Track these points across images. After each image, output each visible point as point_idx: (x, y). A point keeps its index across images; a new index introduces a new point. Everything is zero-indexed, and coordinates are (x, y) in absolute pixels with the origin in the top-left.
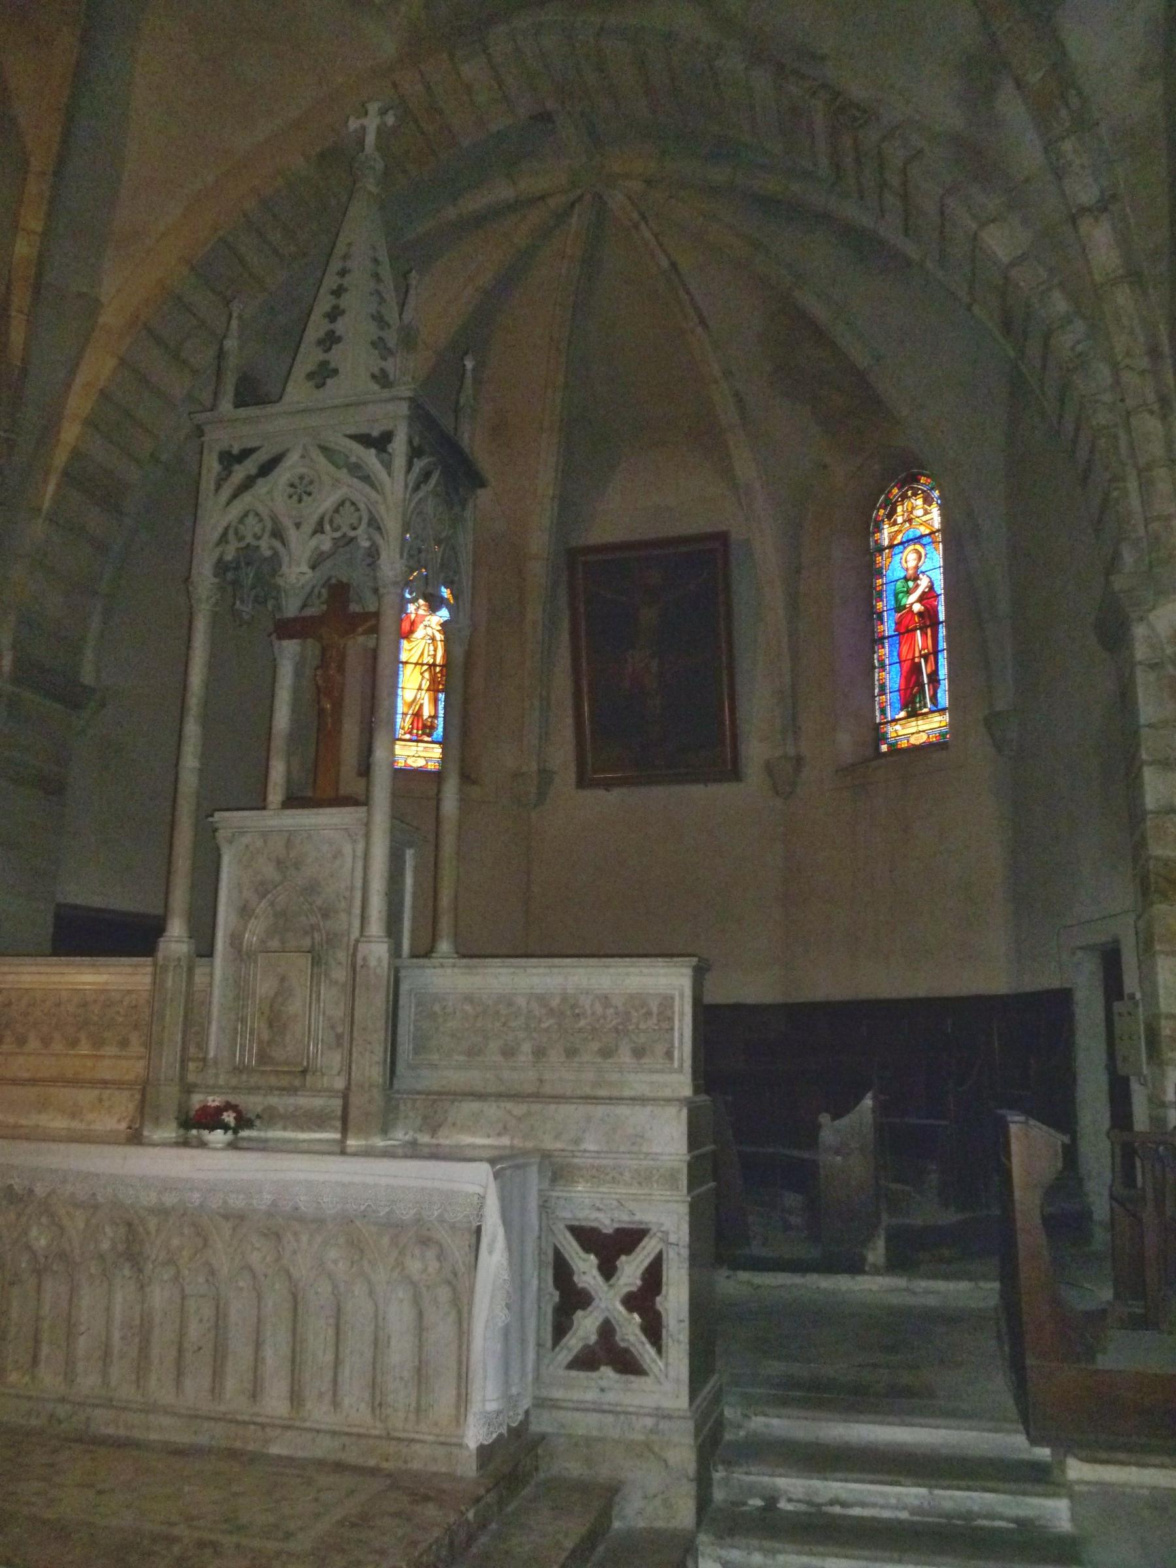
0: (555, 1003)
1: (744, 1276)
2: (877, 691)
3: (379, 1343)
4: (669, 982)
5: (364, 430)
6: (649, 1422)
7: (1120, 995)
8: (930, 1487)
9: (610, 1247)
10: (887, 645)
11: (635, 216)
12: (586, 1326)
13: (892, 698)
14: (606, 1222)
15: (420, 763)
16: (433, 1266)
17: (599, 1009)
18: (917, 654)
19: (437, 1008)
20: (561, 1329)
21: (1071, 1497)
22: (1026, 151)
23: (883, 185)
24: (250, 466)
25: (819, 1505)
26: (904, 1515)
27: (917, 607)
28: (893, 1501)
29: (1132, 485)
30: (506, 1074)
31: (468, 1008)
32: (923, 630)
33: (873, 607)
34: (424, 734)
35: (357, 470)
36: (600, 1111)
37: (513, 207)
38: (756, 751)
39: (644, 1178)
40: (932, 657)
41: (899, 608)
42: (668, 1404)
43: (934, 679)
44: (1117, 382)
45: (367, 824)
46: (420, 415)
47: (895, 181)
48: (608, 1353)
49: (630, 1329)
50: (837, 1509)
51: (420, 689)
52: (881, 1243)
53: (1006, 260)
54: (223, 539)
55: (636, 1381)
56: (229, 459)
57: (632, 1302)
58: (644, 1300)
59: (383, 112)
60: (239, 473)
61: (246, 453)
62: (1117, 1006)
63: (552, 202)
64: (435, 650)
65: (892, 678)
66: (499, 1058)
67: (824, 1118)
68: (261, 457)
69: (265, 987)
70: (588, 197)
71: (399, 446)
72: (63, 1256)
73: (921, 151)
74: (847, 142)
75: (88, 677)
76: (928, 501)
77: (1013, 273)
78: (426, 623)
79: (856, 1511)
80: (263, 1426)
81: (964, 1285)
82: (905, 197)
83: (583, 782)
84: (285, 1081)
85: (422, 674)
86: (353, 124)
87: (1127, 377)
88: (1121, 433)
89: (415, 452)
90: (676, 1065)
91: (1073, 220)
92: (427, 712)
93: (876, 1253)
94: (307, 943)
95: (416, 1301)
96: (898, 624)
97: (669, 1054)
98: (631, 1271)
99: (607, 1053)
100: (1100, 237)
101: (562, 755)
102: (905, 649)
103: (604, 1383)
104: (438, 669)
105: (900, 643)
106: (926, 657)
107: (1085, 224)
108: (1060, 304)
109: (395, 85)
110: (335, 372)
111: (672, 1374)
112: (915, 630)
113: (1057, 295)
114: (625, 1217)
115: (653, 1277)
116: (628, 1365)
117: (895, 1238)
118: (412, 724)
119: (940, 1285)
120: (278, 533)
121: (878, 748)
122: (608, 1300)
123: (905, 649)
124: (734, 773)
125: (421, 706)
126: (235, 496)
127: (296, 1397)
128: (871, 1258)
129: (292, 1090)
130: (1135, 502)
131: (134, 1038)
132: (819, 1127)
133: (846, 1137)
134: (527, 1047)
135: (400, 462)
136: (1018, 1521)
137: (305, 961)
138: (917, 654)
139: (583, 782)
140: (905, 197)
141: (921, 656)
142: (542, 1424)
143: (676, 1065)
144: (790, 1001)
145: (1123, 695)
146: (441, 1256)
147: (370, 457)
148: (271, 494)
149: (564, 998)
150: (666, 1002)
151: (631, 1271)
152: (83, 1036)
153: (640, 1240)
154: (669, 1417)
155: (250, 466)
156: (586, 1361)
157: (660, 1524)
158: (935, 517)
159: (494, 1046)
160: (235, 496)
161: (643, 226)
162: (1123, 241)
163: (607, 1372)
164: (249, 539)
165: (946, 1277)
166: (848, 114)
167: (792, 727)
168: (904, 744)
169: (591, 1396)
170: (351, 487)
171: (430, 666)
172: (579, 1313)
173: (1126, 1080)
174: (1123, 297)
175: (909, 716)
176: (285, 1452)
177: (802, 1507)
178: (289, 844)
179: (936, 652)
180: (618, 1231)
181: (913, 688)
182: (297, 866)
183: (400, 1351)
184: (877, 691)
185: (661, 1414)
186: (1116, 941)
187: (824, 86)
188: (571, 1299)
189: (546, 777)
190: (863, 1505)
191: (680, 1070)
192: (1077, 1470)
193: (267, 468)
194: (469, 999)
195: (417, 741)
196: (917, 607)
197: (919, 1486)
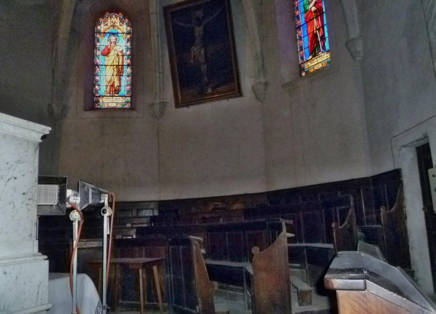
2: (299, 50)
10: (302, 29)
15: (114, 105)
18: (315, 29)
32: (317, 18)
33: (295, 14)
34: (115, 93)
38: (247, 83)
40: (321, 29)
41: (306, 11)
43: (323, 38)
51: (113, 75)
64: (119, 60)
65: (306, 42)
78: (114, 49)
83: (178, 105)
85: (113, 69)
92: (117, 84)
96: (306, 18)
101: (169, 94)
102: (309, 28)
104: (120, 67)
105: (307, 27)
106: (319, 29)
112: (313, 19)
118: (110, 89)
121: (301, 75)
123: (309, 28)
124: (239, 93)
125: (114, 82)
138: (315, 29)
139: (178, 105)
141: (317, 29)
144: (269, 190)
167: (263, 69)
168: (312, 70)
171: (117, 66)
175: (314, 56)
179: (323, 27)
181: (314, 44)
184: (299, 50)
189: (163, 105)
195: (112, 96)
196: (314, 9)
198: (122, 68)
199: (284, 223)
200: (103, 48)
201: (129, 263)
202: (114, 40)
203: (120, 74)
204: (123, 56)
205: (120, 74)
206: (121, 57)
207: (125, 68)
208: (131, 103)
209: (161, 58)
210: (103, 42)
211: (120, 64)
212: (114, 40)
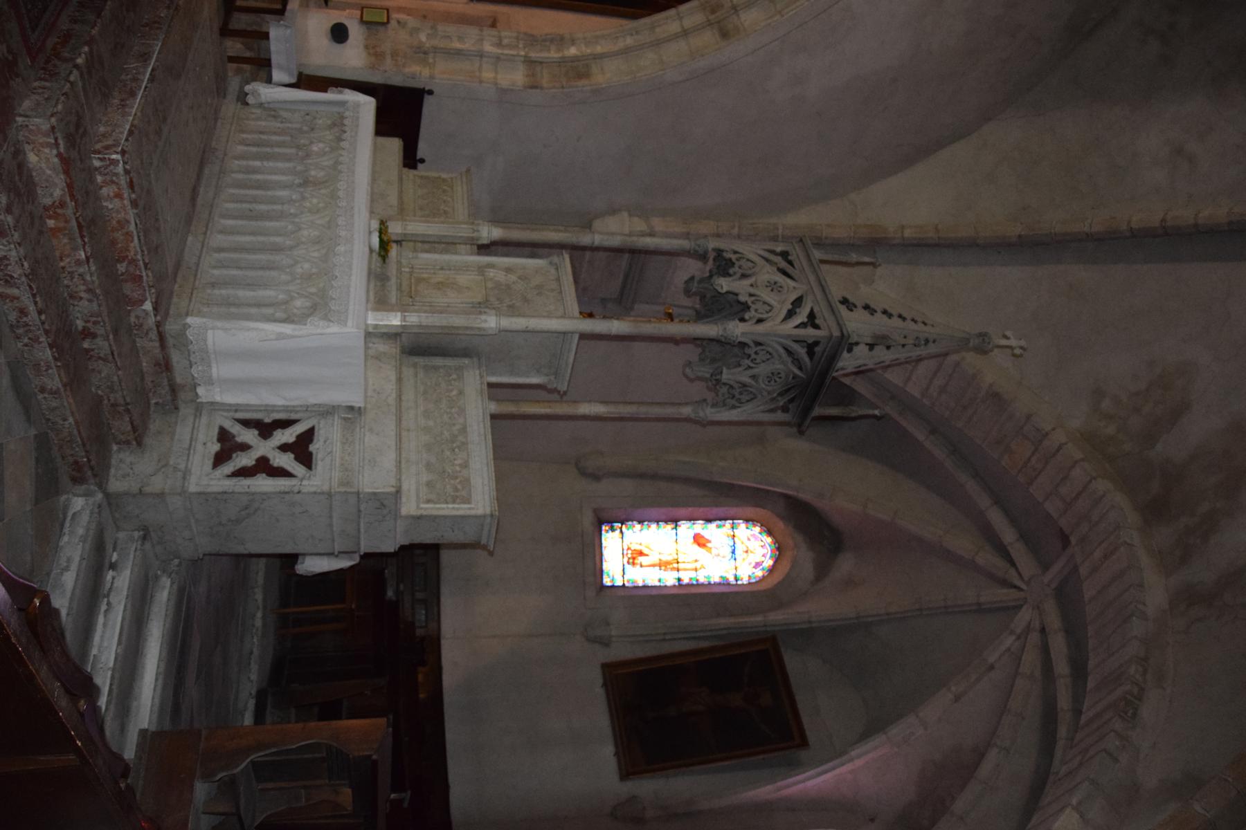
0: (461, 438)
1: (251, 704)
3: (250, 285)
4: (481, 500)
5: (818, 315)
6: (182, 466)
8: (114, 670)
9: (302, 449)
11: (1018, 631)
12: (249, 436)
19: (454, 376)
20: (246, 423)
24: (783, 264)
25: (108, 596)
26: (94, 651)
28: (105, 644)
31: (454, 393)
37: (1002, 550)
48: (228, 447)
49: (245, 460)
50: (104, 607)
55: (209, 462)
56: (785, 255)
58: (264, 467)
60: (778, 259)
61: (790, 263)
63: (1012, 571)
68: (789, 269)
69: (463, 279)
71: (810, 331)
72: (308, 156)
73: (1116, 760)
79: (101, 619)
80: (205, 233)
83: (607, 667)
89: (811, 348)
90: (423, 506)
97: (428, 501)
98: (285, 461)
99: (428, 466)
103: (209, 444)
109: (1054, 429)
111: (212, 483)
114: (320, 456)
120: (744, 276)
122: (265, 448)
129: (399, 288)
134: (431, 423)
135: (802, 332)
139: (607, 667)
143: (423, 506)
147: (802, 317)
148: (768, 274)
153: (302, 462)
154: (184, 478)
156: (224, 436)
157: (113, 471)
161: (1014, 637)
163: (216, 447)
164: (737, 264)
169: (201, 437)
172: (256, 432)
176: (188, 243)
177: (108, 586)
180: (311, 454)
185: (186, 474)
187: (1142, 689)
188: (266, 429)
190: (105, 625)
191: (418, 507)
197: (116, 659)
198: (673, 569)
199: (407, 795)
200: (703, 533)
201: (695, 321)
202: (728, 553)
203: (663, 565)
204: (696, 570)
205: (663, 565)
206: (693, 566)
207: (675, 574)
208: (613, 586)
209: (1064, 702)
210: (716, 533)
211: (681, 566)
212: (728, 553)
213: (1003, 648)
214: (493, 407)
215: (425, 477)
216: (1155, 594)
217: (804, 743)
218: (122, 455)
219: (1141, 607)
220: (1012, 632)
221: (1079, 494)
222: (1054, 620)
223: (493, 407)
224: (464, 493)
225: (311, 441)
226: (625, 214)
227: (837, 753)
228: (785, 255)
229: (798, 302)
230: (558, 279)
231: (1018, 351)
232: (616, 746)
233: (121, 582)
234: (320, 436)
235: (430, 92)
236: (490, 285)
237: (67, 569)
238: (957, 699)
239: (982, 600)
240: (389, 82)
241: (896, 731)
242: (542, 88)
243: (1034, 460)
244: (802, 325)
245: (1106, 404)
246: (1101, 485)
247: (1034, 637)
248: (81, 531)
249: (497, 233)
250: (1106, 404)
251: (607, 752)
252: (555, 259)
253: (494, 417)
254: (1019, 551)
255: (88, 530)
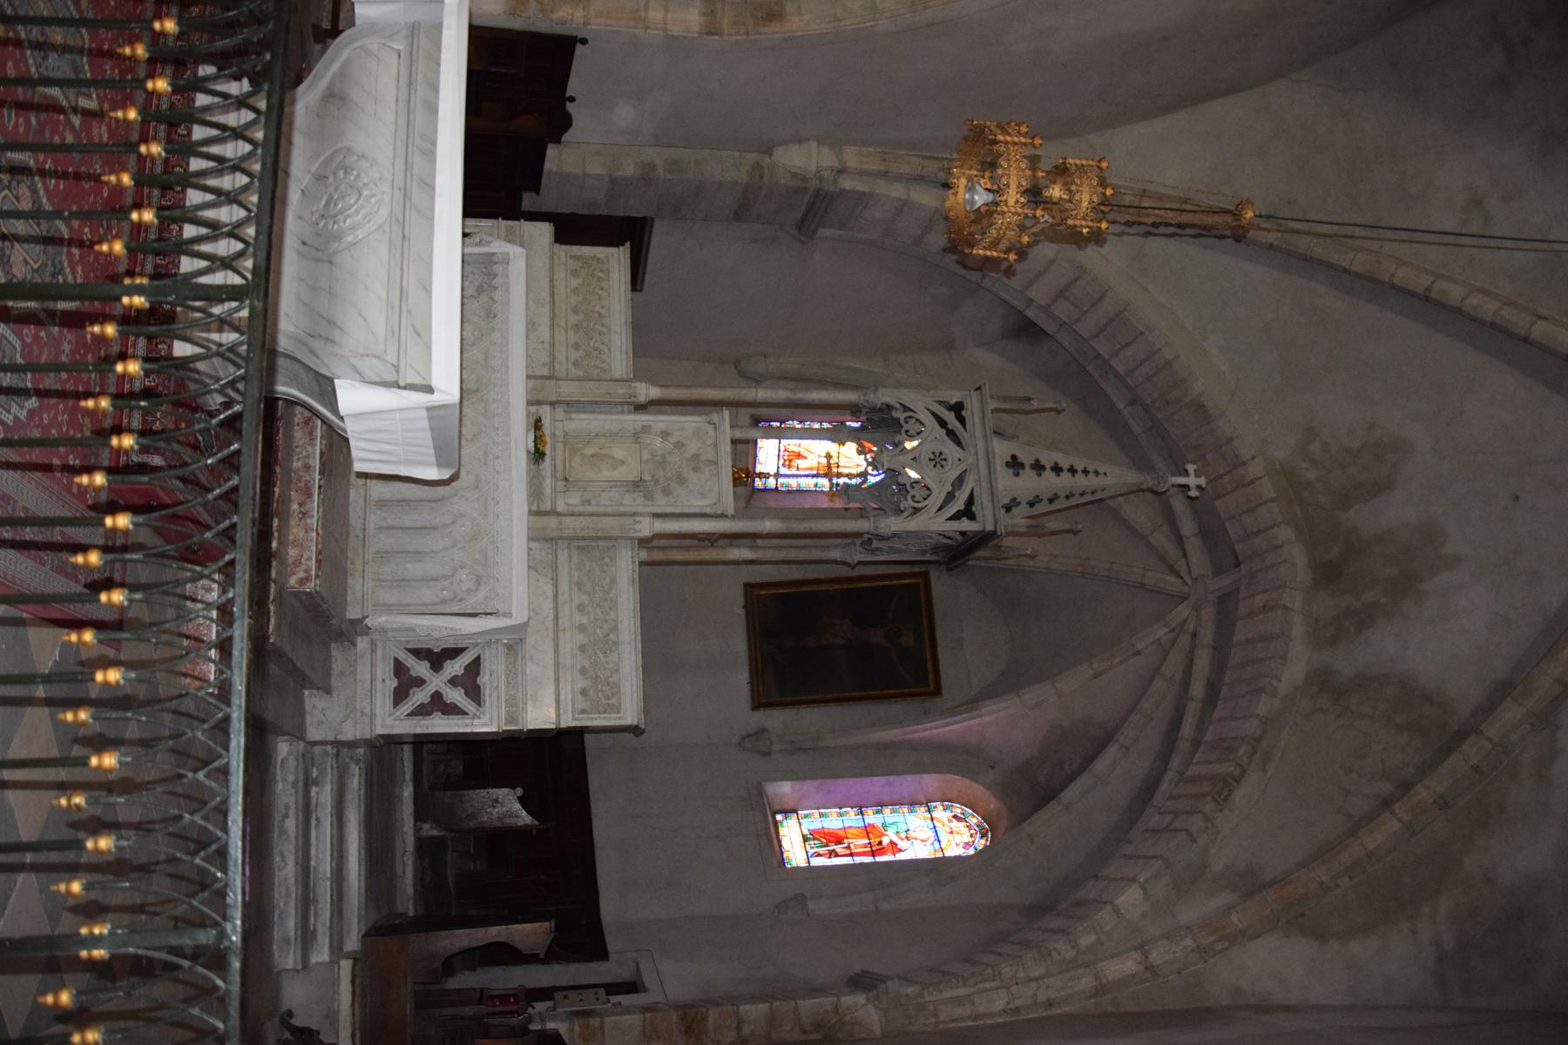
0: (612, 636)
3: (419, 555)
5: (977, 501)
7: (609, 993)
9: (470, 682)
11: (1173, 625)
12: (420, 668)
13: (816, 824)
14: (483, 680)
16: (464, 587)
17: (611, 665)
20: (417, 653)
21: (332, 962)
22: (1191, 913)
23: (1176, 814)
24: (953, 423)
27: (885, 841)
29: (961, 992)
30: (567, 608)
35: (950, 497)
36: (551, 673)
37: (1179, 540)
38: (776, 719)
39: (511, 702)
42: (378, 721)
44: (1031, 980)
45: (723, 516)
46: (985, 538)
47: (1177, 824)
48: (405, 684)
49: (420, 696)
52: (435, 833)
53: (1118, 902)
54: (906, 409)
55: (389, 701)
57: (437, 696)
58: (438, 704)
59: (1199, 487)
60: (950, 417)
61: (962, 420)
62: (602, 991)
63: (1183, 562)
66: (576, 602)
67: (519, 791)
69: (618, 452)
70: (1186, 589)
71: (966, 525)
73: (1194, 841)
74: (1206, 788)
75: (824, 232)
76: (967, 845)
77: (1109, 908)
81: (410, 891)
82: (1167, 830)
83: (748, 586)
84: (560, 467)
86: (1191, 468)
87: (1033, 985)
88: (998, 983)
91: (1140, 947)
92: (802, 463)
93: (429, 830)
94: (647, 477)
95: (445, 577)
96: (873, 826)
97: (583, 711)
98: (455, 696)
99: (583, 671)
100: (1128, 965)
107: (1136, 955)
108: (1086, 940)
109: (1253, 458)
110: (1017, 475)
113: (1093, 937)
115: (452, 710)
116: (400, 696)
117: (439, 842)
119: (410, 874)
121: (779, 812)
124: (759, 704)
126: (934, 414)
127: (382, 504)
128: (426, 826)
130: (949, 993)
131: (580, 353)
132: (513, 787)
133: (506, 806)
134: (585, 620)
136: (315, 930)
137: (633, 476)
139: (748, 586)
140: (1167, 830)
142: (362, 643)
145: (816, 990)
146: (469, 591)
147: (959, 505)
149: (616, 643)
150: (617, 709)
151: (455, 696)
152: (581, 317)
155: (953, 423)
156: (400, 669)
157: (308, 719)
158: (952, 852)
159: (585, 598)
160: (934, 414)
162: (1124, 982)
163: (395, 683)
164: (906, 427)
165: (415, 877)
166: (1224, 788)
169: (379, 673)
170: (938, 497)
173: (551, 998)
174: (1086, 982)
178: (709, 462)
179: (851, 855)
182: (696, 469)
183: (414, 569)
186: (645, 991)
187: (1244, 772)
190: (317, 838)
192: (346, 966)
193: (951, 434)
194: (613, 580)
196: (885, 841)
213: (1153, 638)
214: (644, 555)
215: (581, 683)
216: (1296, 664)
217: (937, 692)
218: (314, 700)
219: (1275, 683)
220: (1166, 625)
221: (1259, 532)
222: (1207, 635)
223: (644, 555)
224: (613, 701)
225: (478, 673)
226: (814, 145)
227: (972, 703)
228: (958, 408)
229: (960, 480)
230: (715, 445)
231: (1193, 493)
232: (751, 673)
233: (324, 796)
234: (486, 666)
235: (584, 41)
236: (646, 456)
237: (286, 816)
238: (1097, 675)
239: (1146, 581)
240: (533, 29)
241: (1030, 695)
242: (721, 35)
243: (1226, 478)
244: (957, 517)
245: (1315, 448)
246: (1284, 534)
247: (1185, 640)
248: (292, 778)
249: (655, 392)
250: (1315, 448)
251: (740, 680)
252: (715, 418)
253: (642, 564)
254: (1194, 546)
255: (296, 774)
